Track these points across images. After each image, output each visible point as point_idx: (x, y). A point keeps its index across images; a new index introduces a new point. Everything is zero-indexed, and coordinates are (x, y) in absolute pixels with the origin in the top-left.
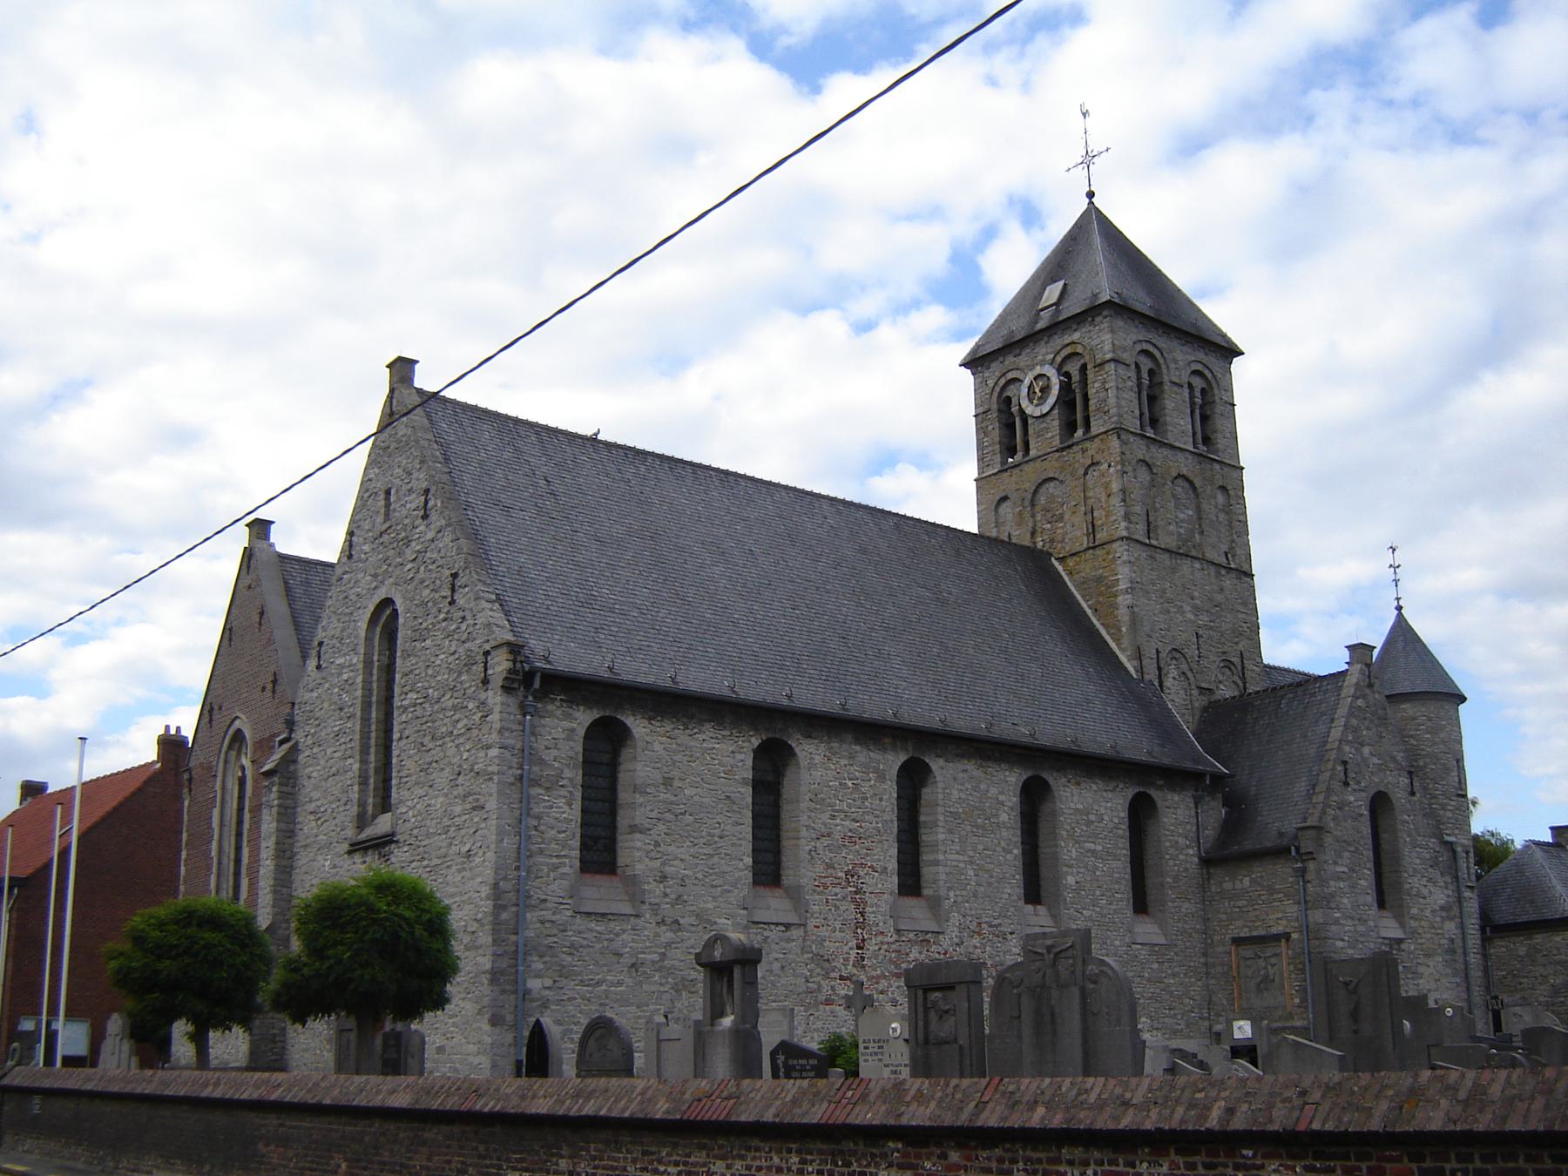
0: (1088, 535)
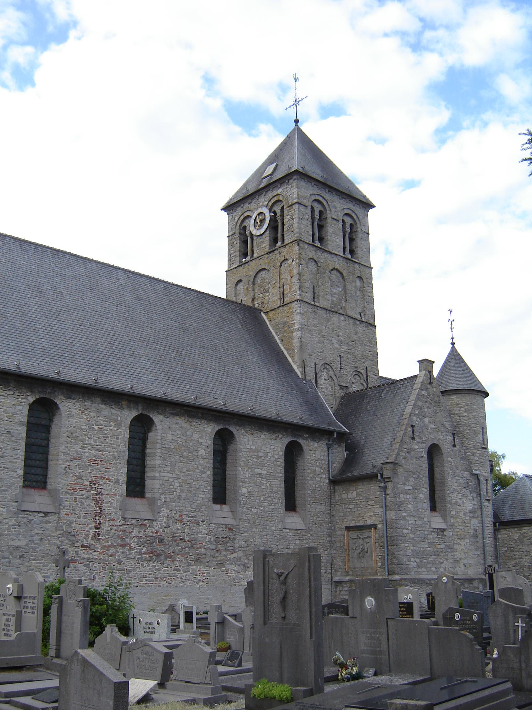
0: (280, 299)
